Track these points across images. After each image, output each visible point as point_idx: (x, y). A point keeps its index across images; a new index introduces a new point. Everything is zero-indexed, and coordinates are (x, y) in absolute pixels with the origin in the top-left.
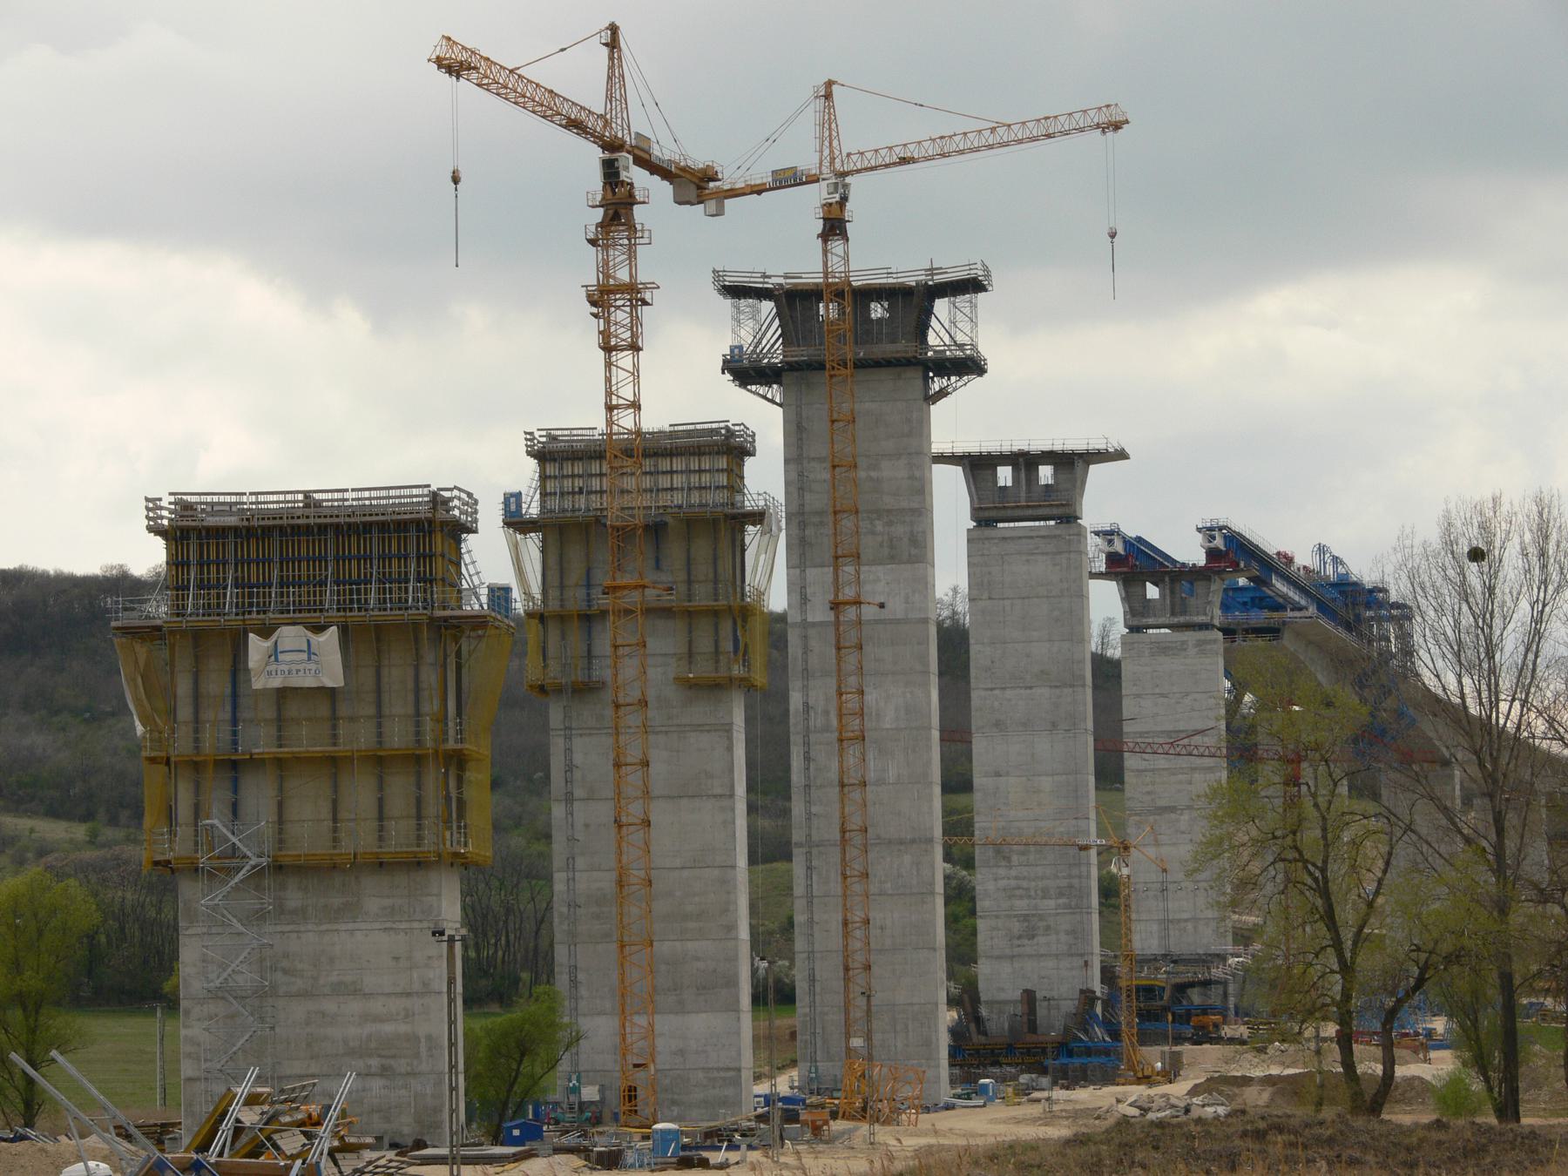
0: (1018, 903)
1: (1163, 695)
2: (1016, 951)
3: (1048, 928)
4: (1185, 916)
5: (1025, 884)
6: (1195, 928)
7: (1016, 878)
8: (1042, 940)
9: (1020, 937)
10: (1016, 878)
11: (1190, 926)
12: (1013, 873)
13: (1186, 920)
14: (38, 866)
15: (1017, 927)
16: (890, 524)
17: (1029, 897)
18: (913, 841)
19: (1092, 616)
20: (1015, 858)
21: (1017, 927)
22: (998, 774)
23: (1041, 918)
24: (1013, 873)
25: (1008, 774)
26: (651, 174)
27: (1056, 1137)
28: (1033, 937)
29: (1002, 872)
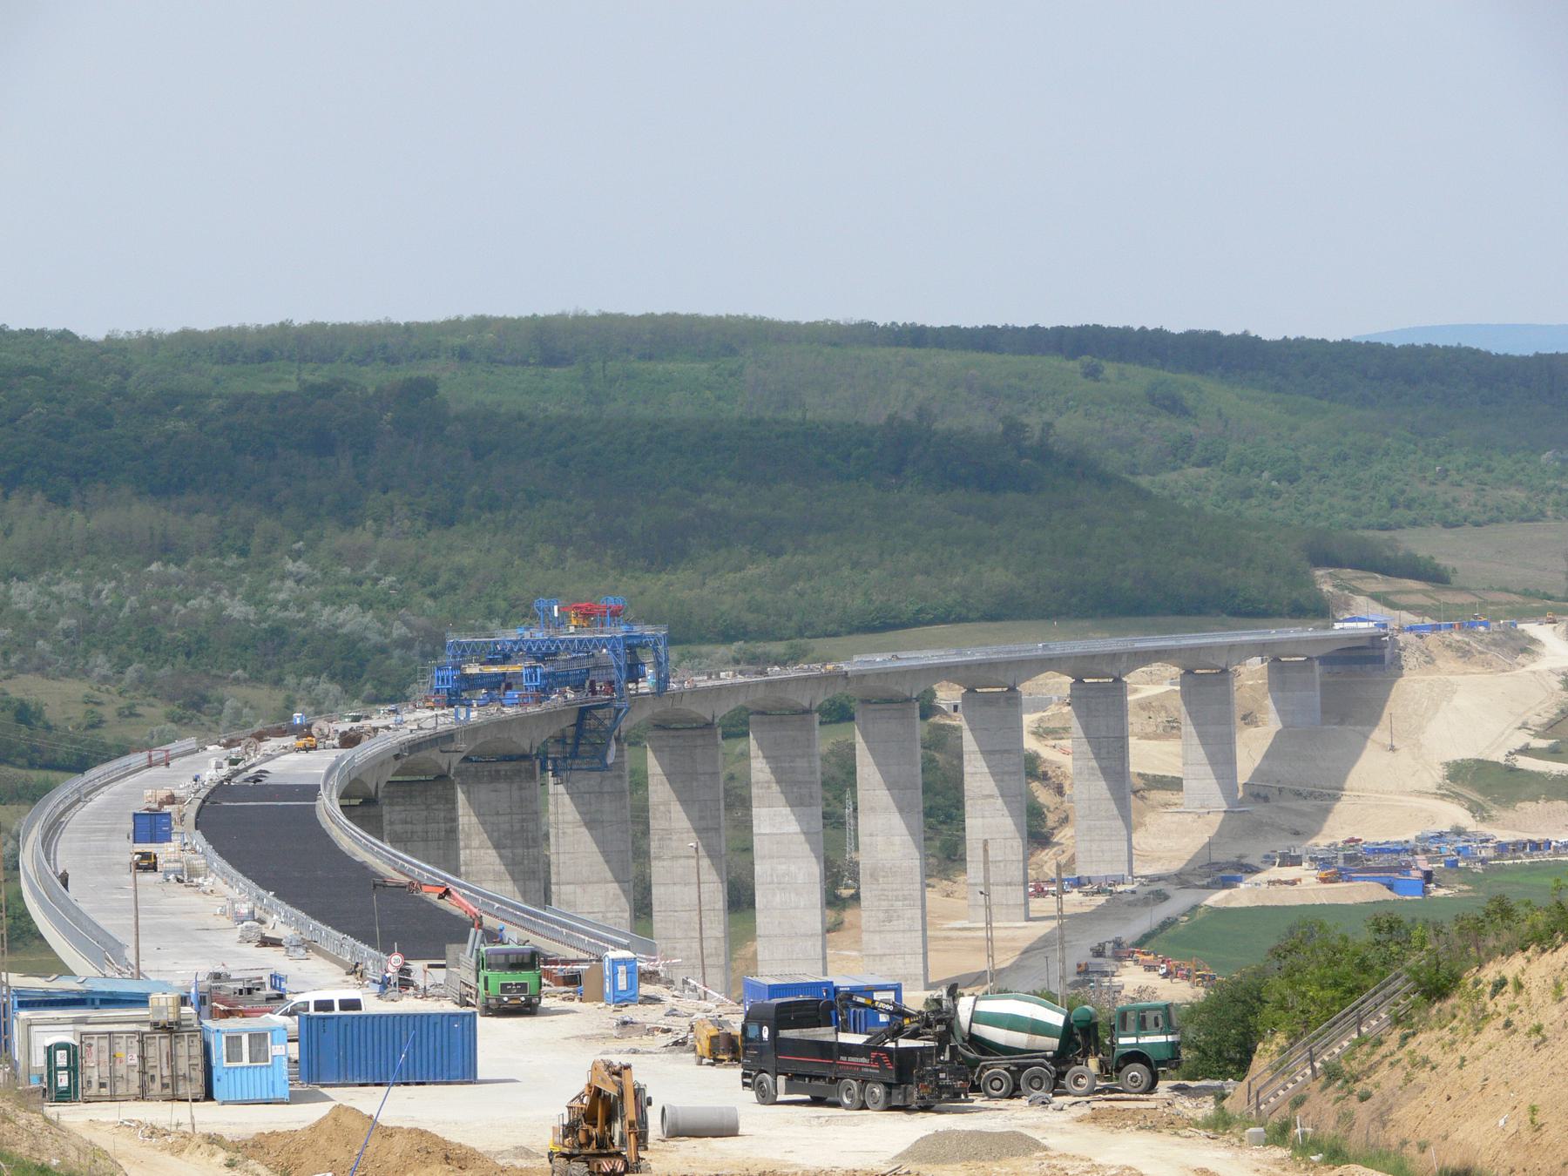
0: (883, 903)
1: (986, 729)
2: (882, 928)
3: (898, 916)
4: (1000, 859)
5: (886, 893)
6: (1005, 866)
7: (882, 890)
8: (895, 923)
9: (884, 921)
10: (882, 890)
11: (1002, 865)
12: (880, 887)
13: (1000, 861)
14: (1337, 990)
15: (881, 915)
16: (800, 788)
17: (888, 900)
18: (812, 935)
19: (896, 821)
20: (881, 880)
21: (881, 915)
22: (871, 835)
23: (895, 911)
24: (880, 887)
25: (877, 835)
26: (535, 315)
27: (1555, 773)
28: (890, 921)
29: (875, 887)
